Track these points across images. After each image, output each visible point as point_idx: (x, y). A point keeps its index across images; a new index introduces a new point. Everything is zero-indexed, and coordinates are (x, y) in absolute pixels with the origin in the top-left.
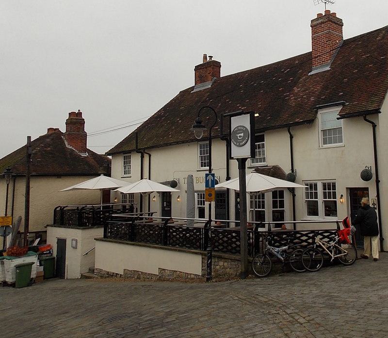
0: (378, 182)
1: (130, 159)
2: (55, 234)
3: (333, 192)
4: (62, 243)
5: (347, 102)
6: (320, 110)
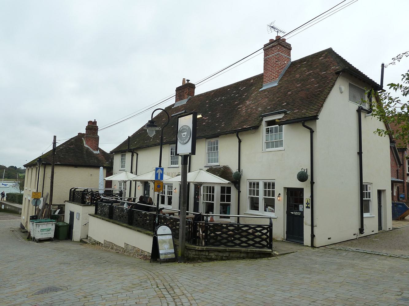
0: (312, 183)
1: (125, 156)
2: (70, 207)
3: (256, 190)
4: (72, 214)
5: (288, 111)
6: (265, 118)
